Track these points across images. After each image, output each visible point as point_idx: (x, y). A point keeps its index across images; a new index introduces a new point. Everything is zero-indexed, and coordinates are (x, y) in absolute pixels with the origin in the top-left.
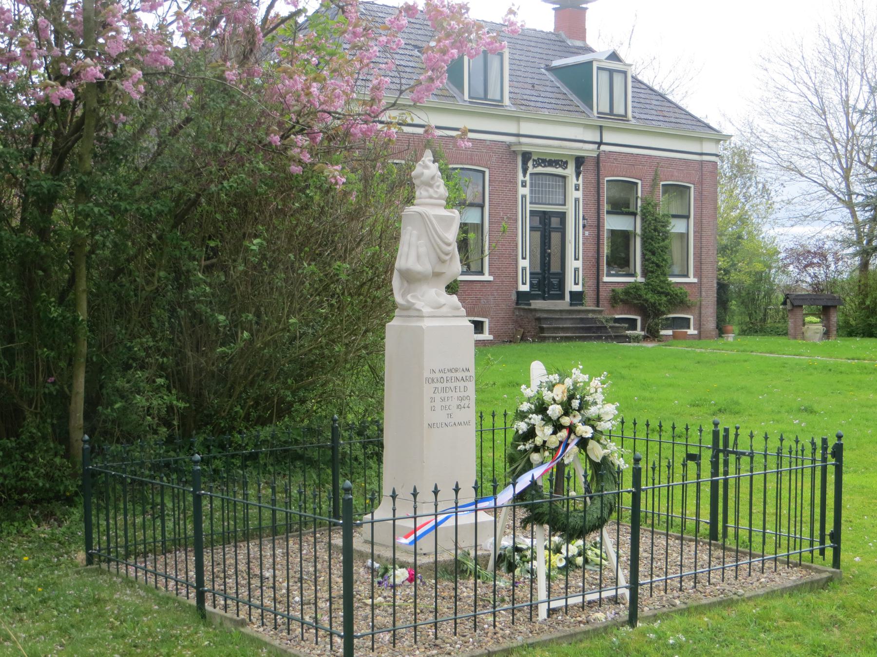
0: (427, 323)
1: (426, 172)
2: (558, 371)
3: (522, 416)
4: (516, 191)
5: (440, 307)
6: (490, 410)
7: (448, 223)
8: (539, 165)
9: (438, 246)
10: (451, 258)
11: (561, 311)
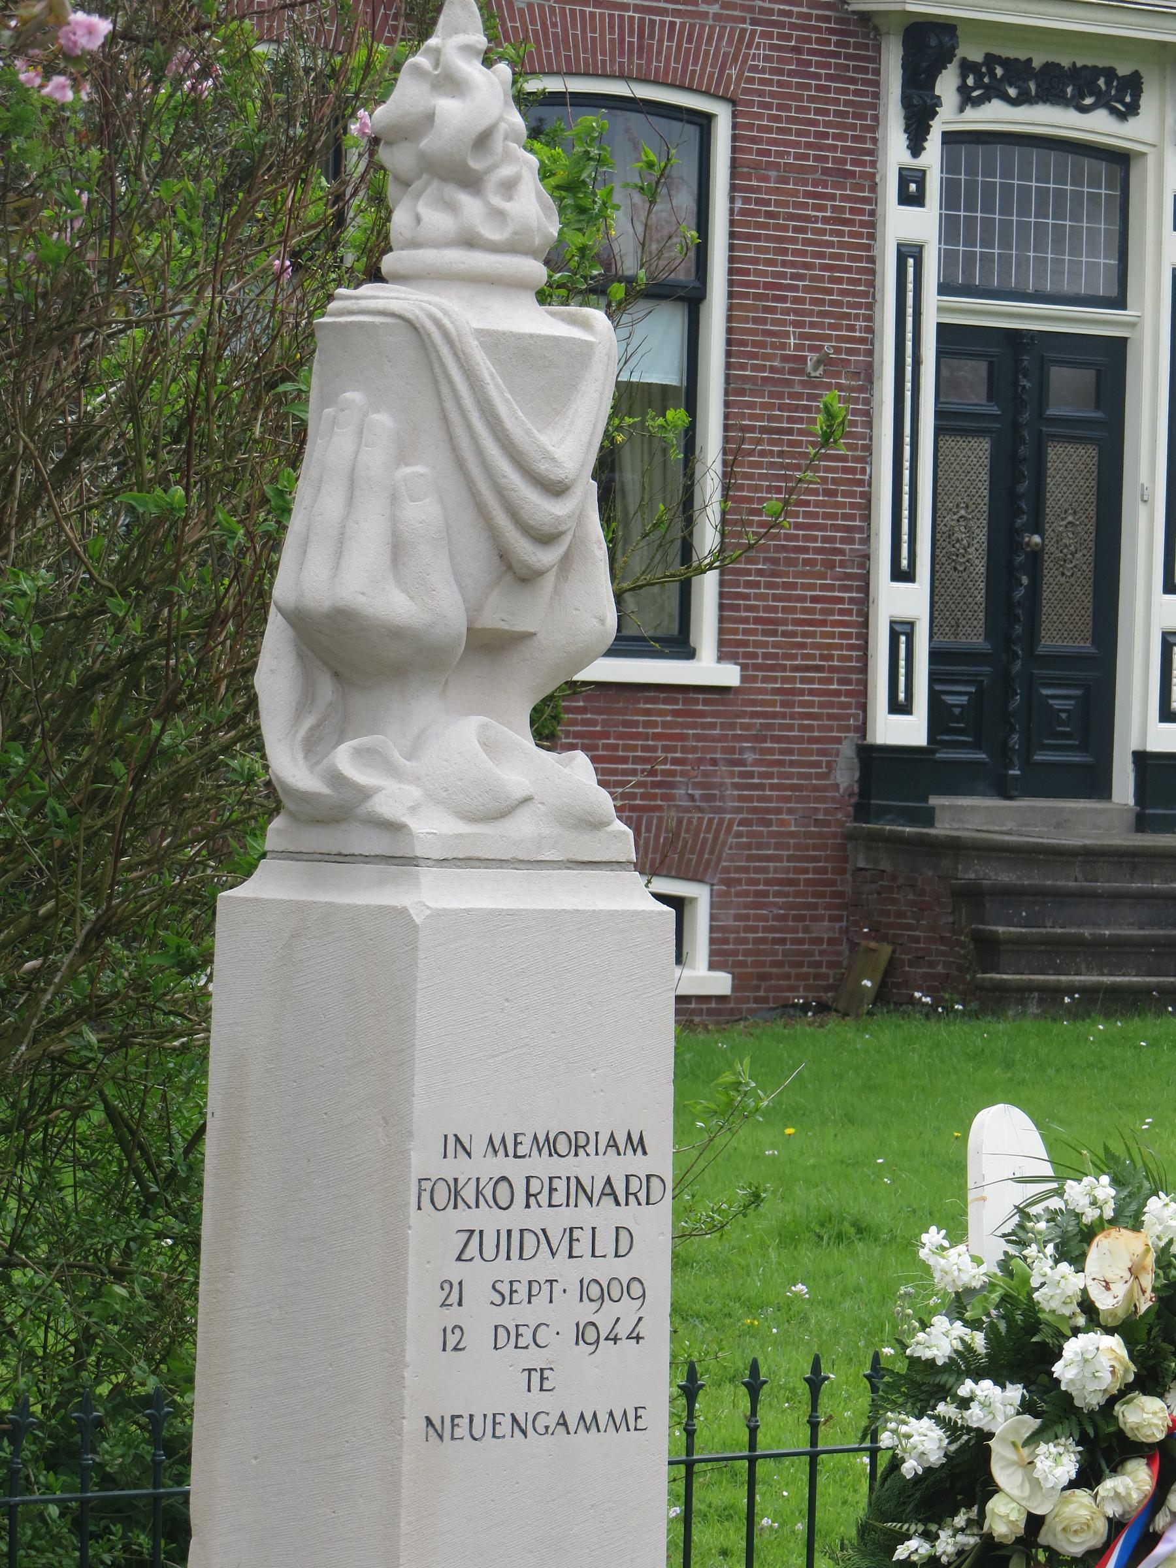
0: (431, 896)
1: (448, 108)
2: (1109, 1164)
3: (925, 1387)
4: (872, 226)
5: (502, 811)
6: (738, 1362)
7: (562, 377)
8: (993, 92)
9: (501, 492)
10: (566, 562)
11: (1090, 856)
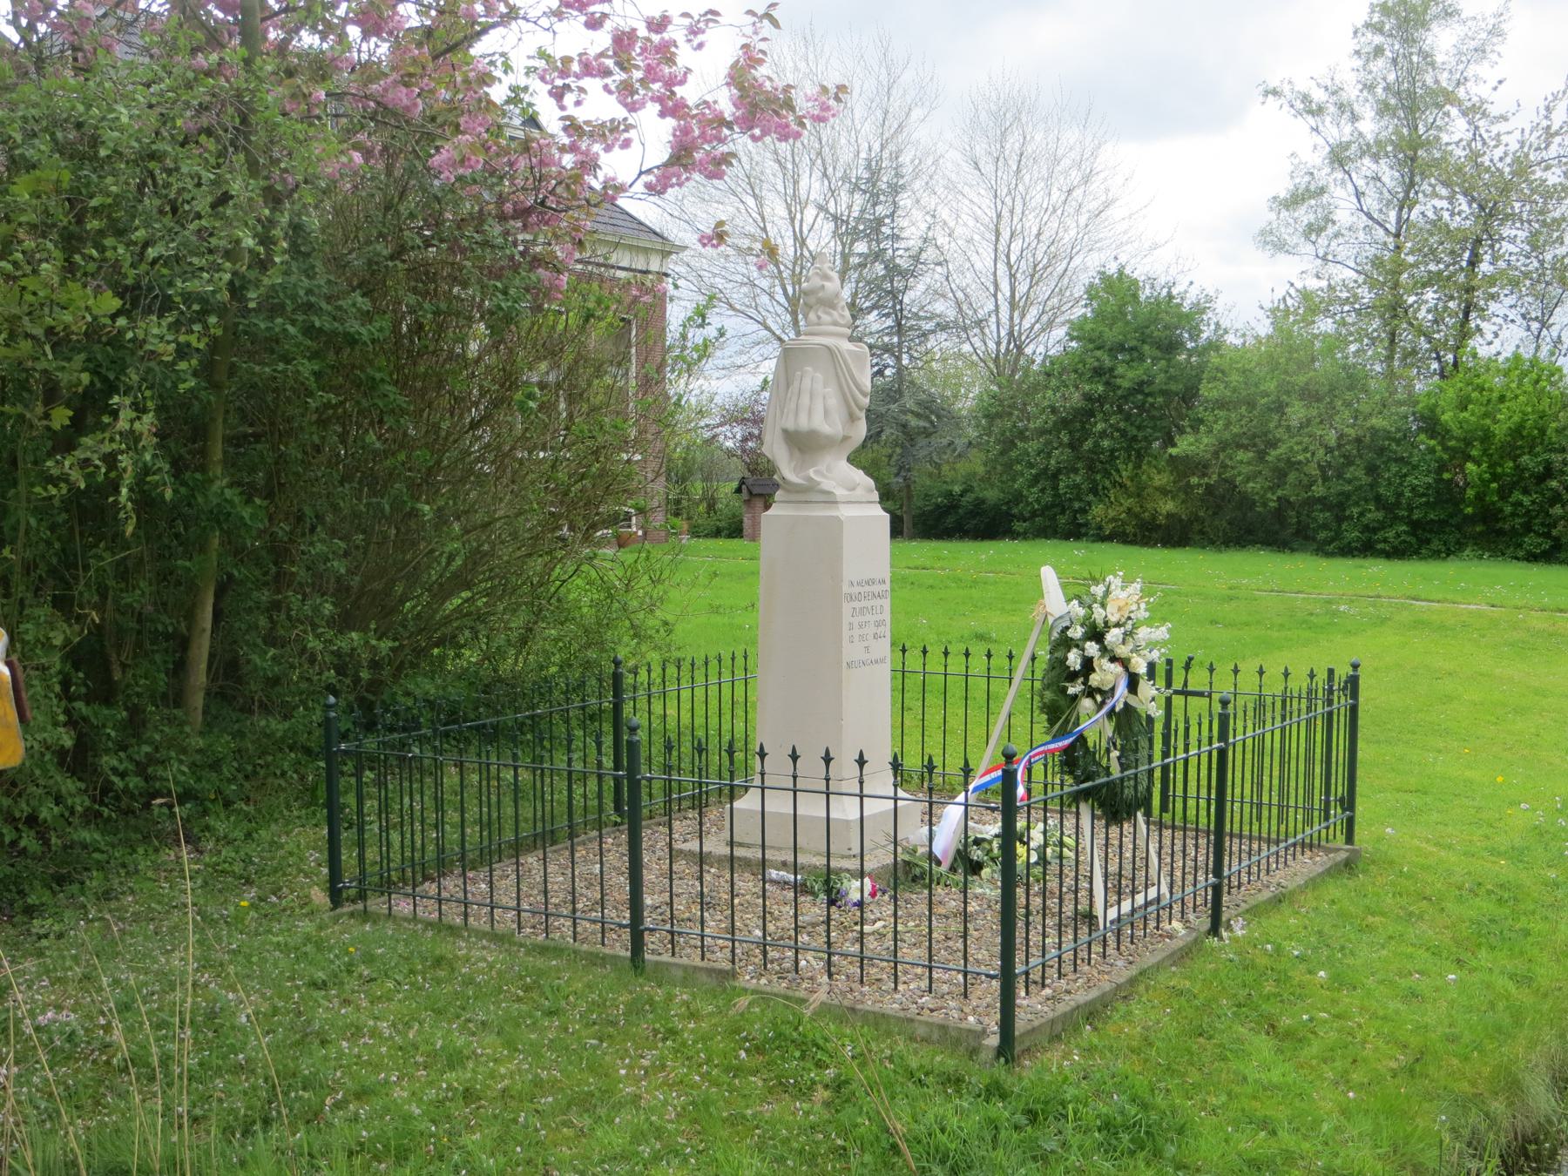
0: (845, 512)
